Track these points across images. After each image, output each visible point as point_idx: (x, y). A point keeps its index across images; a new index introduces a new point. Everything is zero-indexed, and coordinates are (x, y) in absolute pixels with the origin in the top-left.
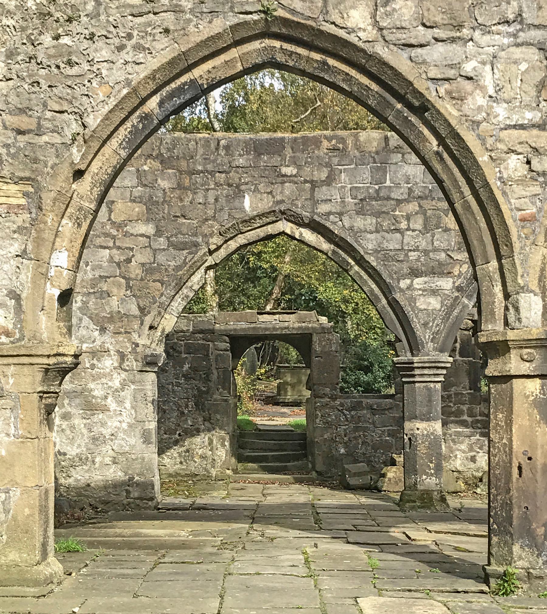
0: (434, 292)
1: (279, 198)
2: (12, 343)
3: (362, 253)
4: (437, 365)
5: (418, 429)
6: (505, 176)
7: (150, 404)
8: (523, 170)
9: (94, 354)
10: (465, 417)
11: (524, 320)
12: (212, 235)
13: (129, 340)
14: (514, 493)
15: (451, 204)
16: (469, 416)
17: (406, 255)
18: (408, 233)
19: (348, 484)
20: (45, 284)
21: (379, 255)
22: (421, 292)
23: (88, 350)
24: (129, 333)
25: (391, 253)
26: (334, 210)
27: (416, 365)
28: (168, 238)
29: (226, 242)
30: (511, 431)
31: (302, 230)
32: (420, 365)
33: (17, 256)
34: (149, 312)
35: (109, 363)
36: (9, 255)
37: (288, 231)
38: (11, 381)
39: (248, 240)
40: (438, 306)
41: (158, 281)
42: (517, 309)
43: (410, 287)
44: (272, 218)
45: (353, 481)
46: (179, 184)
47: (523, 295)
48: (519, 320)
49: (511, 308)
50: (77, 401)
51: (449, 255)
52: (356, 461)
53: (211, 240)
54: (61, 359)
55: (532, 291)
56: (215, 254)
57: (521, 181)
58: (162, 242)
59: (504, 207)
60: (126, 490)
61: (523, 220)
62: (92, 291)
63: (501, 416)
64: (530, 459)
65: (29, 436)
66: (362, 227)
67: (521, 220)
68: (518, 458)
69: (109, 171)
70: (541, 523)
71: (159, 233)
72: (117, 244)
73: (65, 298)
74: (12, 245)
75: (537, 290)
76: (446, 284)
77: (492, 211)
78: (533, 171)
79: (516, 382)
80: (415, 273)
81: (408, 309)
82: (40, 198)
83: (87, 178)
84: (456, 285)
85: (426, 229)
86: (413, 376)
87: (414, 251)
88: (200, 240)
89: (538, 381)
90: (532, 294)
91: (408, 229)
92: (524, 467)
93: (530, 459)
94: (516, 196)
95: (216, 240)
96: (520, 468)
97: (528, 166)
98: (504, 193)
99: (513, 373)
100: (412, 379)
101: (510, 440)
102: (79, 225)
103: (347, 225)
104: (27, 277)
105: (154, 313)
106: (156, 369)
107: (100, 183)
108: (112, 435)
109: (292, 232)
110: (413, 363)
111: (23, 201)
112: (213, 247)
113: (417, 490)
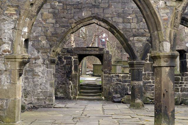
0: (140, 41)
1: (93, 12)
2: (10, 54)
3: (118, 29)
4: (142, 64)
5: (135, 84)
6: (159, 7)
7: (52, 75)
8: (164, 6)
9: (36, 59)
10: (150, 80)
11: (165, 50)
12: (72, 23)
13: (47, 55)
14: (162, 102)
15: (143, 15)
16: (152, 80)
17: (132, 30)
18: (132, 24)
19: (114, 101)
20: (21, 37)
21: (124, 30)
22: (136, 42)
23: (34, 58)
24: (47, 53)
25: (127, 30)
26: (110, 16)
27: (135, 64)
28: (59, 24)
29: (77, 25)
30: (161, 83)
31: (100, 22)
32: (136, 64)
33: (13, 29)
34: (53, 47)
35: (40, 61)
36: (10, 28)
37: (96, 22)
38: (9, 66)
39: (84, 25)
40: (142, 46)
41: (56, 37)
42: (163, 46)
43: (133, 40)
44: (91, 18)
45: (115, 100)
46: (63, 8)
47: (164, 42)
48: (163, 50)
49: (161, 46)
50: (30, 73)
51: (145, 30)
52: (116, 93)
53: (72, 25)
54: (24, 60)
55: (167, 41)
56: (73, 29)
57: (164, 8)
58: (58, 25)
59: (158, 16)
60: (45, 102)
61: (164, 20)
62: (36, 40)
63: (158, 79)
64: (167, 92)
65: (14, 83)
66: (118, 21)
67: (164, 20)
68: (163, 91)
69: (41, 4)
70: (170, 111)
71: (57, 22)
72: (44, 26)
73: (27, 41)
74: (11, 25)
75: (169, 41)
76: (144, 39)
77: (155, 17)
78: (167, 6)
79: (162, 68)
80: (134, 36)
81: (132, 46)
82: (20, 11)
83: (34, 6)
84: (147, 39)
85: (138, 23)
86: (134, 67)
87: (134, 29)
88: (69, 24)
89: (169, 68)
90: (167, 42)
91: (132, 22)
92: (165, 94)
93: (167, 92)
94: (162, 13)
95: (73, 25)
96: (164, 95)
97: (165, 4)
98: (158, 12)
99: (162, 66)
100: (134, 68)
101: (161, 86)
102: (31, 20)
103: (114, 21)
104: (15, 35)
105: (55, 47)
106: (55, 64)
107: (38, 7)
108: (41, 84)
109: (97, 22)
110: (134, 63)
111: (15, 12)
112: (73, 27)
113: (135, 103)
